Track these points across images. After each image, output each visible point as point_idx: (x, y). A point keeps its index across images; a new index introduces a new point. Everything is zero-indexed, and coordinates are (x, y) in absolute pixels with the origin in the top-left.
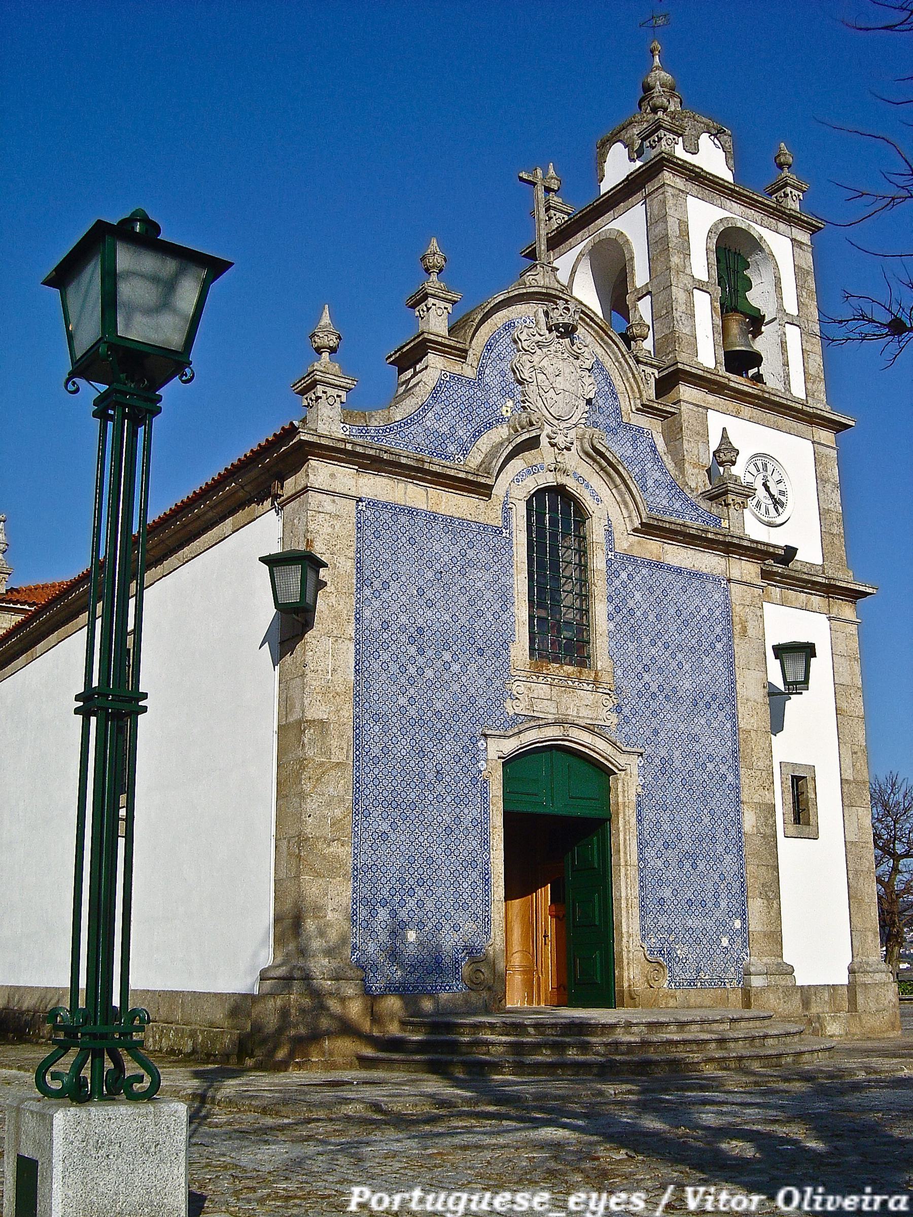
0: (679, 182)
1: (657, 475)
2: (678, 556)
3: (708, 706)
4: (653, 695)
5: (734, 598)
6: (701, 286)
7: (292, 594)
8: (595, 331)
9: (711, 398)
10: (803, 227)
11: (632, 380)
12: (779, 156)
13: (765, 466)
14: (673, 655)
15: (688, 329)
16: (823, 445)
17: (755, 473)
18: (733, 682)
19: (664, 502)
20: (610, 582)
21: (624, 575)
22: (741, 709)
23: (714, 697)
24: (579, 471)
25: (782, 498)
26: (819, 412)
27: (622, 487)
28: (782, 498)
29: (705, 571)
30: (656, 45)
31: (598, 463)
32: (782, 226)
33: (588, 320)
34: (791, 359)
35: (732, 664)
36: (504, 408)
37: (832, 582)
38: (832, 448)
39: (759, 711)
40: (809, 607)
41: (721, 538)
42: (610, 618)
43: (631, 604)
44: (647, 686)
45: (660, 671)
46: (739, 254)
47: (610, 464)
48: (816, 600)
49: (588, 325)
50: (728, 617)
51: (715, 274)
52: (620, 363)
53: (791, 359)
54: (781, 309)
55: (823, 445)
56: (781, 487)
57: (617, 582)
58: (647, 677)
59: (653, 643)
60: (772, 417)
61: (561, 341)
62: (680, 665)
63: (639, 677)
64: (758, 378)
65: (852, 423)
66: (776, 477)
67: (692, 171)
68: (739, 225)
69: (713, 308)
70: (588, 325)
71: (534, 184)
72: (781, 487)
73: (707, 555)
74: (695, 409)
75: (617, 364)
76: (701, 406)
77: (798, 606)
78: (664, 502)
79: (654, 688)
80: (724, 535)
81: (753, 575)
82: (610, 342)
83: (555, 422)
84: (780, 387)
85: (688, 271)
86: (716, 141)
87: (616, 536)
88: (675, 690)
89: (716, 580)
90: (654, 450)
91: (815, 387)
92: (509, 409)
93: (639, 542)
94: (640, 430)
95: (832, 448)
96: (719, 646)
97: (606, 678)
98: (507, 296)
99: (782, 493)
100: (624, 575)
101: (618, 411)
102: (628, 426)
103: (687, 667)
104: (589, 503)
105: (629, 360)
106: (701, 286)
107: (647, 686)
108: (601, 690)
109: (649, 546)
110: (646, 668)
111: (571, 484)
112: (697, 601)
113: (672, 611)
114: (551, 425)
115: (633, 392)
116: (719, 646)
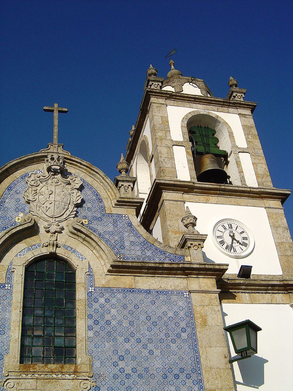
0: (162, 101)
1: (132, 239)
2: (145, 282)
3: (177, 377)
4: (128, 376)
5: (194, 303)
6: (178, 144)
7: (243, 343)
8: (85, 170)
9: (186, 196)
10: (245, 107)
11: (110, 190)
12: (229, 82)
13: (231, 227)
14: (145, 347)
15: (170, 164)
16: (272, 208)
17: (223, 230)
18: (198, 358)
19: (139, 253)
20: (90, 306)
21: (102, 300)
22: (205, 376)
23: (182, 370)
24: (68, 244)
25: (245, 241)
26: (263, 190)
27: (97, 247)
28: (245, 241)
29: (170, 289)
30: (172, 61)
31: (80, 237)
32: (231, 110)
33: (79, 165)
34: (247, 168)
35: (196, 346)
36: (17, 218)
37: (285, 282)
38: (279, 208)
39: (222, 374)
40: (274, 302)
41: (175, 266)
42: (90, 328)
43: (108, 317)
44: (122, 370)
45: (134, 358)
46: (208, 127)
47: (86, 235)
48: (279, 297)
49: (80, 167)
50: (190, 314)
51: (187, 137)
52: (102, 183)
53: (247, 168)
54: (234, 146)
55: (272, 208)
56: (244, 235)
57: (96, 306)
58: (121, 364)
59: (127, 340)
60: (233, 199)
61: (56, 176)
62: (151, 352)
63: (115, 365)
64: (231, 183)
65: (290, 192)
66: (239, 230)
67: (166, 94)
68: (202, 113)
69: (187, 152)
70: (80, 167)
71: (53, 111)
72: (244, 235)
73: (171, 279)
74: (175, 203)
75: (101, 184)
76: (179, 201)
77: (265, 302)
78: (139, 253)
79: (128, 370)
80: (177, 264)
81: (210, 285)
82: (95, 173)
83: (50, 219)
84: (239, 184)
85: (168, 138)
86: (194, 85)
87: (96, 277)
88: (147, 370)
89: (180, 293)
90: (130, 225)
91: (263, 180)
92: (20, 218)
93: (115, 279)
94: (119, 216)
95: (279, 208)
96: (184, 335)
97: (84, 368)
98: (19, 160)
99: (245, 238)
100: (102, 300)
101: (103, 208)
102: (111, 215)
103: (157, 352)
104: (74, 260)
105: (106, 179)
106: (178, 144)
107: (122, 370)
108: (80, 378)
109: (123, 280)
110: (121, 358)
111: (60, 252)
112: (164, 308)
113: (143, 317)
114: (47, 221)
115: (112, 196)
116: (184, 335)
